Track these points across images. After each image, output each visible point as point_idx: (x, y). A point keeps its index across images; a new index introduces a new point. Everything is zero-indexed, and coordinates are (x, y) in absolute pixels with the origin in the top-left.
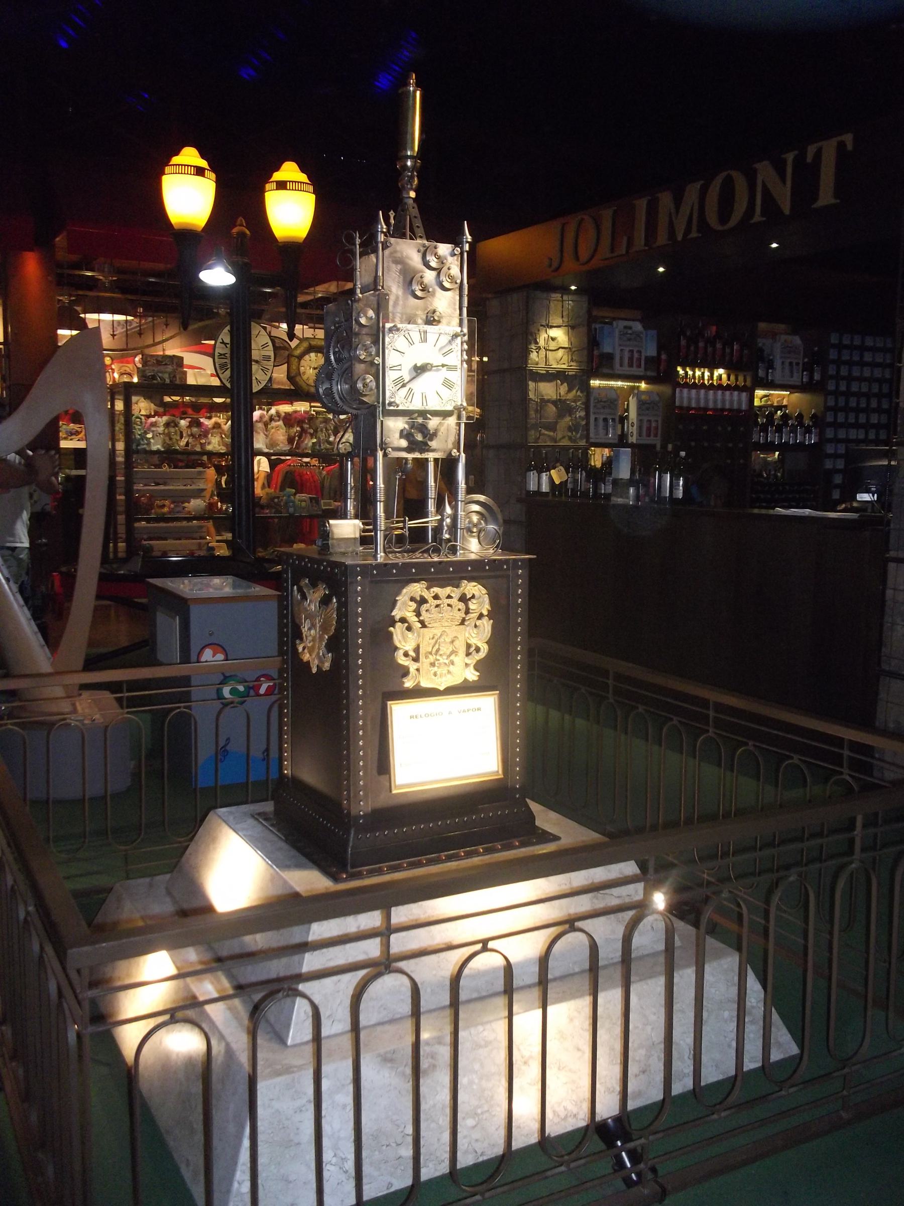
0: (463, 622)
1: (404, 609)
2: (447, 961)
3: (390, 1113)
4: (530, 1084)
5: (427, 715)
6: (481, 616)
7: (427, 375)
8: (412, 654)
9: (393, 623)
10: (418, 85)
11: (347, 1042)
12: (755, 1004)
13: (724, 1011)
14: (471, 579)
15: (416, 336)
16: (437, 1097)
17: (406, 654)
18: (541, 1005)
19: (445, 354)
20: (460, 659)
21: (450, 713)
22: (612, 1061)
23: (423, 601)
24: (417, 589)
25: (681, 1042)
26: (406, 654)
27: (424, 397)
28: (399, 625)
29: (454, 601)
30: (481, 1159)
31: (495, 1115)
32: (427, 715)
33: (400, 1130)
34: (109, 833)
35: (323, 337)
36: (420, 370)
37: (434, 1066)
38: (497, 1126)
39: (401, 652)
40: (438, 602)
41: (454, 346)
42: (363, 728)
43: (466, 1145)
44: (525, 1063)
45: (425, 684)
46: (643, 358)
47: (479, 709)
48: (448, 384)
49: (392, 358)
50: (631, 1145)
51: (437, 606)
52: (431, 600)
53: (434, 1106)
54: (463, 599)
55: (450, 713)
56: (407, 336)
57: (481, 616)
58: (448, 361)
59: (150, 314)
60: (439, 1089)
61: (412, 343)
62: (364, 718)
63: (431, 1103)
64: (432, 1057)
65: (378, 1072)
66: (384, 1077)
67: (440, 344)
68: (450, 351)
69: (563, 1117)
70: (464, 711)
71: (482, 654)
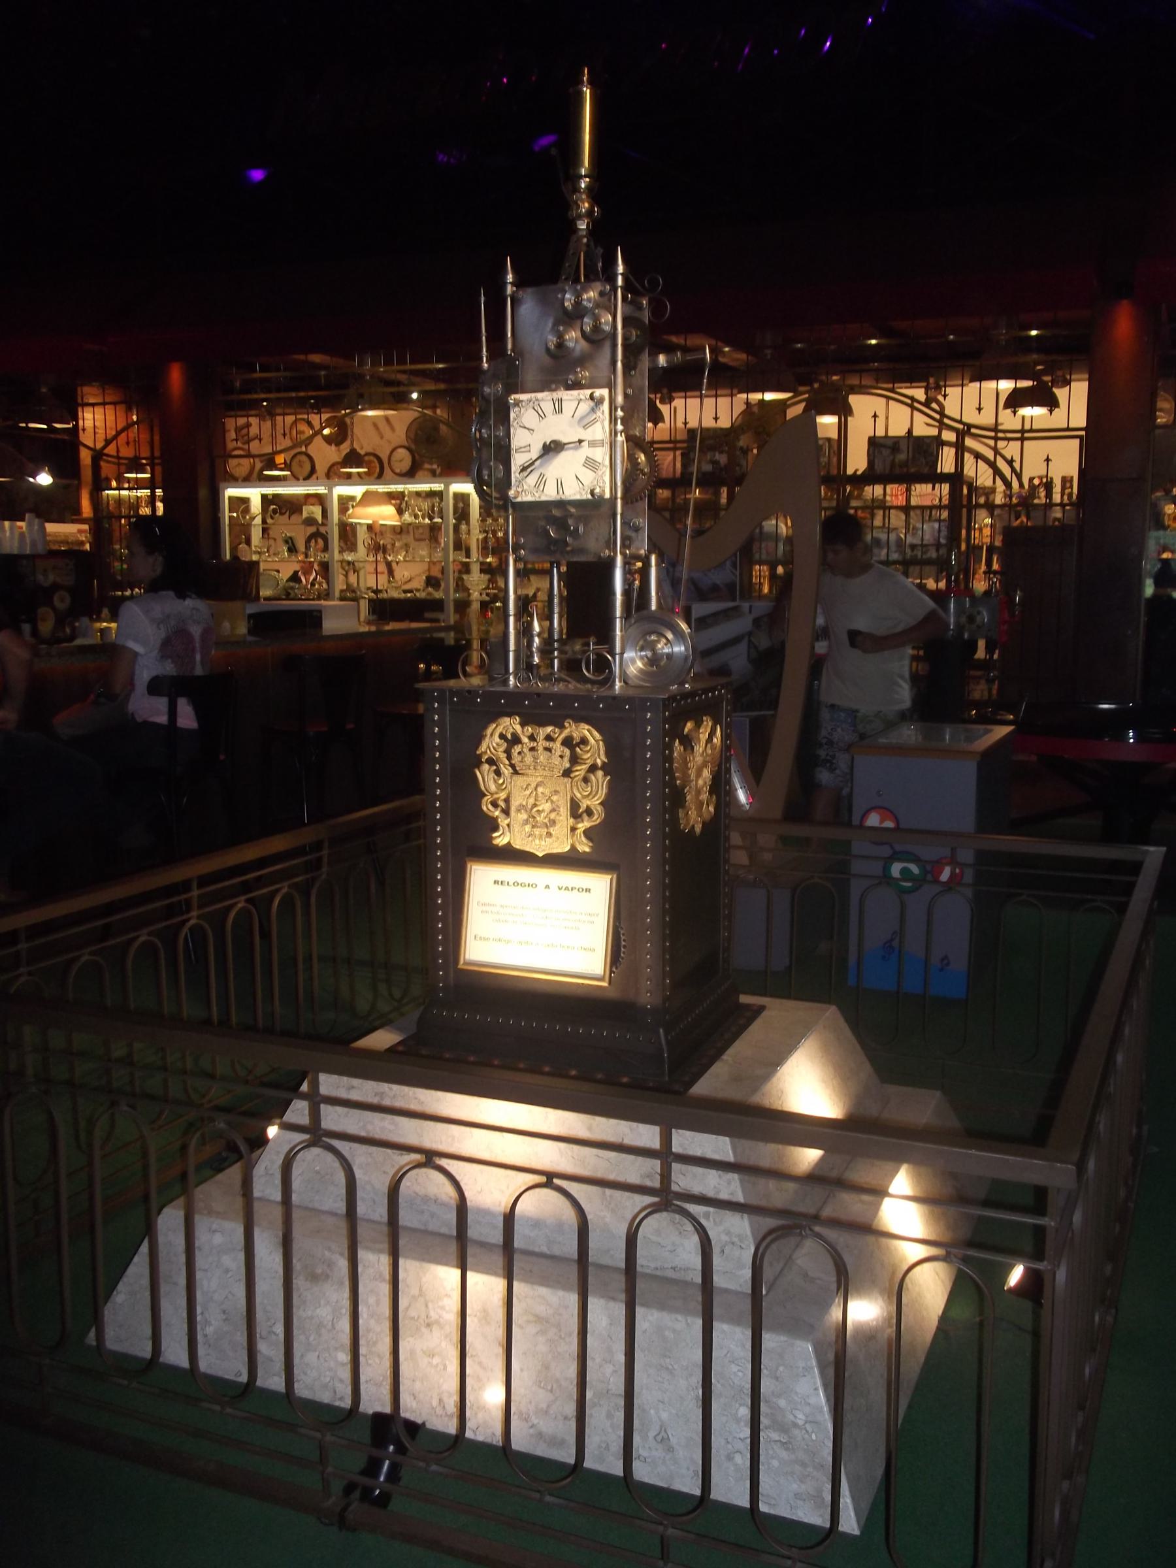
0: (567, 773)
1: (491, 743)
2: (427, 1176)
3: (266, 1301)
4: (424, 1352)
5: (516, 884)
6: (593, 769)
7: (564, 456)
8: (502, 804)
9: (478, 764)
10: (591, 83)
11: (277, 1213)
12: (801, 1423)
13: (741, 1405)
14: (579, 719)
15: (548, 407)
16: (318, 1311)
17: (495, 804)
18: (460, 1265)
19: (585, 427)
20: (564, 819)
21: (547, 887)
22: (540, 1382)
23: (516, 740)
24: (510, 724)
25: (652, 1412)
26: (495, 804)
27: (560, 485)
28: (486, 767)
29: (557, 746)
30: (337, 1403)
31: (370, 1365)
32: (516, 884)
33: (269, 1323)
34: (315, 960)
35: (890, 434)
36: (552, 448)
37: (327, 1277)
38: (368, 1379)
39: (488, 798)
40: (533, 744)
41: (599, 413)
42: (443, 883)
43: (328, 1379)
44: (428, 1325)
45: (518, 845)
46: (402, 389)
47: (588, 890)
48: (590, 464)
49: (519, 438)
50: (399, 1458)
51: (532, 749)
52: (525, 740)
53: (312, 1318)
54: (568, 742)
55: (547, 887)
56: (537, 408)
57: (593, 769)
58: (587, 435)
59: (292, 411)
60: (322, 1302)
61: (542, 416)
62: (442, 871)
63: (310, 1313)
64: (329, 1266)
65: (270, 1253)
66: (274, 1260)
67: (579, 414)
68: (594, 421)
69: (449, 1413)
70: (567, 888)
71: (597, 819)
